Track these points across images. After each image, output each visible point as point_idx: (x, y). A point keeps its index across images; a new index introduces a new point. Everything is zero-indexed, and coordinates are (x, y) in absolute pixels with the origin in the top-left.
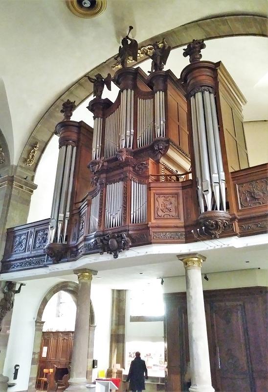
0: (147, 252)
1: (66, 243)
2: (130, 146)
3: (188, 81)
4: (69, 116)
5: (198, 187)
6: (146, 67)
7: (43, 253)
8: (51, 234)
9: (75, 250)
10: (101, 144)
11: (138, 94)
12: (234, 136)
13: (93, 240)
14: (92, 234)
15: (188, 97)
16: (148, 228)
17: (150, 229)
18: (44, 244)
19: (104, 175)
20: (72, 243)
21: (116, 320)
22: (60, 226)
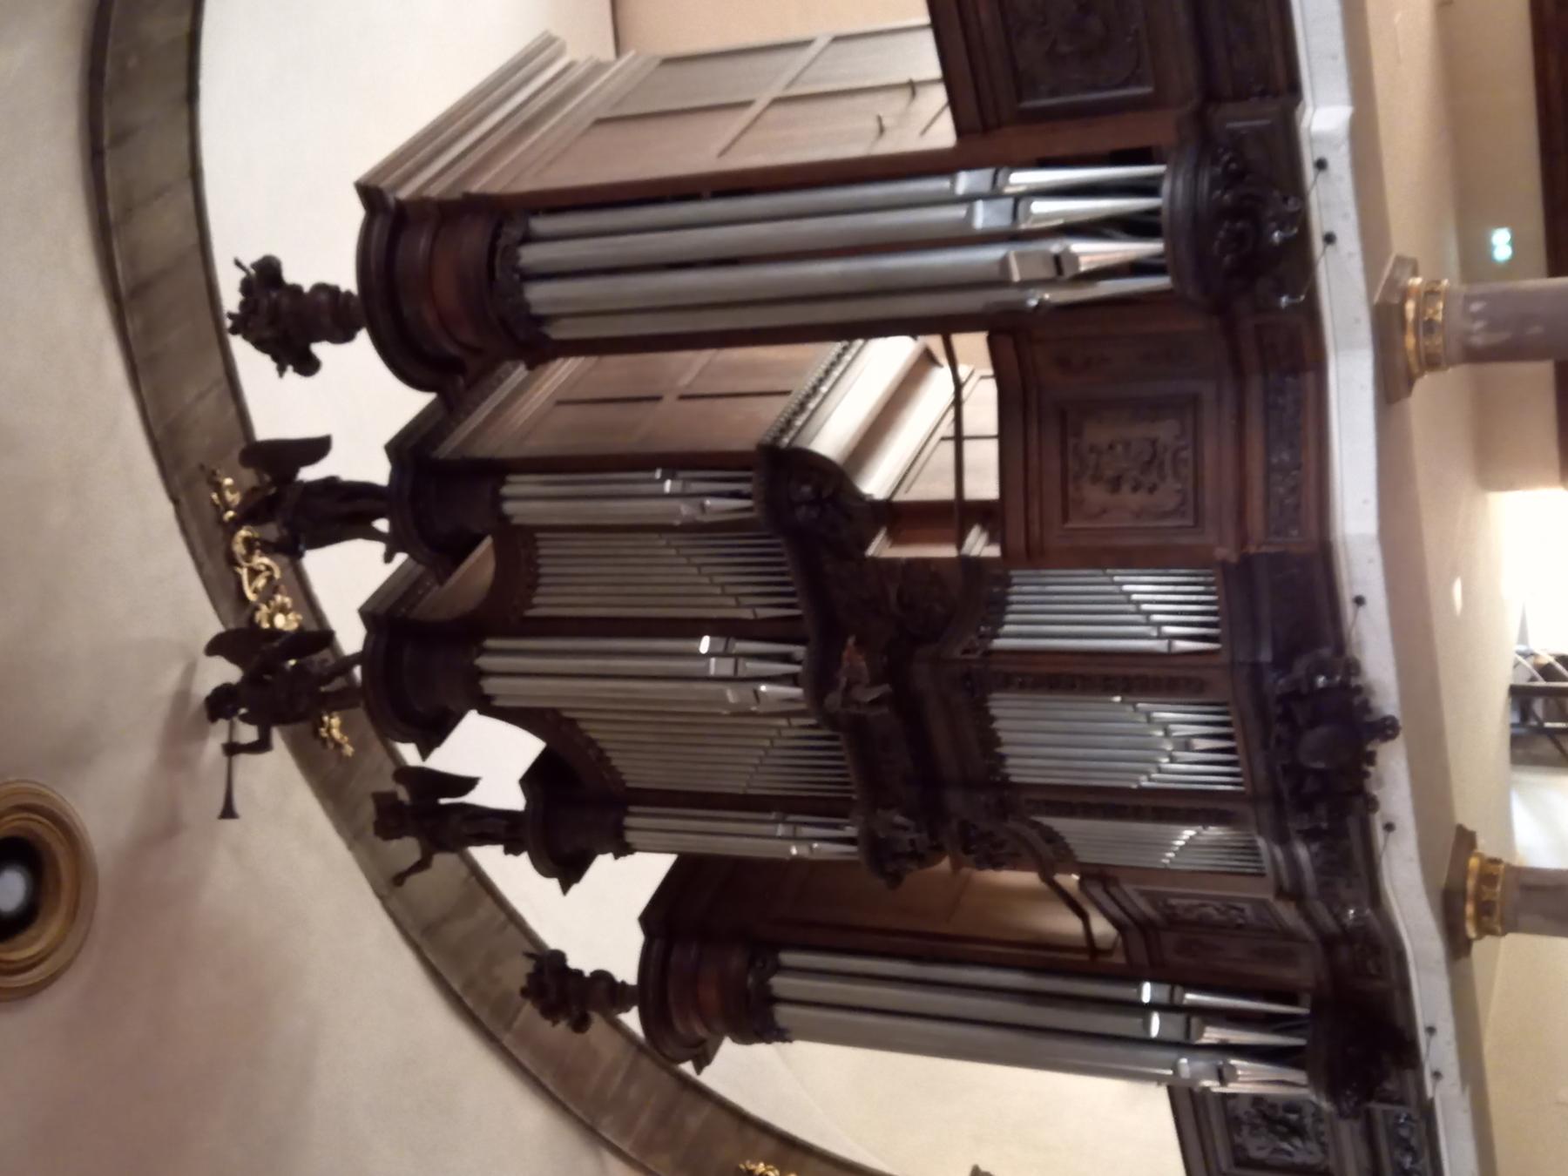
0: (1371, 561)
1: (1307, 998)
2: (786, 658)
3: (452, 350)
4: (601, 991)
5: (1033, 303)
6: (348, 578)
7: (1357, 1125)
8: (1249, 1079)
9: (1344, 954)
10: (773, 816)
11: (508, 614)
12: (748, 115)
13: (1302, 852)
14: (1265, 856)
15: (538, 347)
16: (1246, 562)
17: (1252, 549)
18: (1309, 1110)
19: (955, 800)
20: (1304, 971)
21: (1229, 905)
22: (1212, 1035)
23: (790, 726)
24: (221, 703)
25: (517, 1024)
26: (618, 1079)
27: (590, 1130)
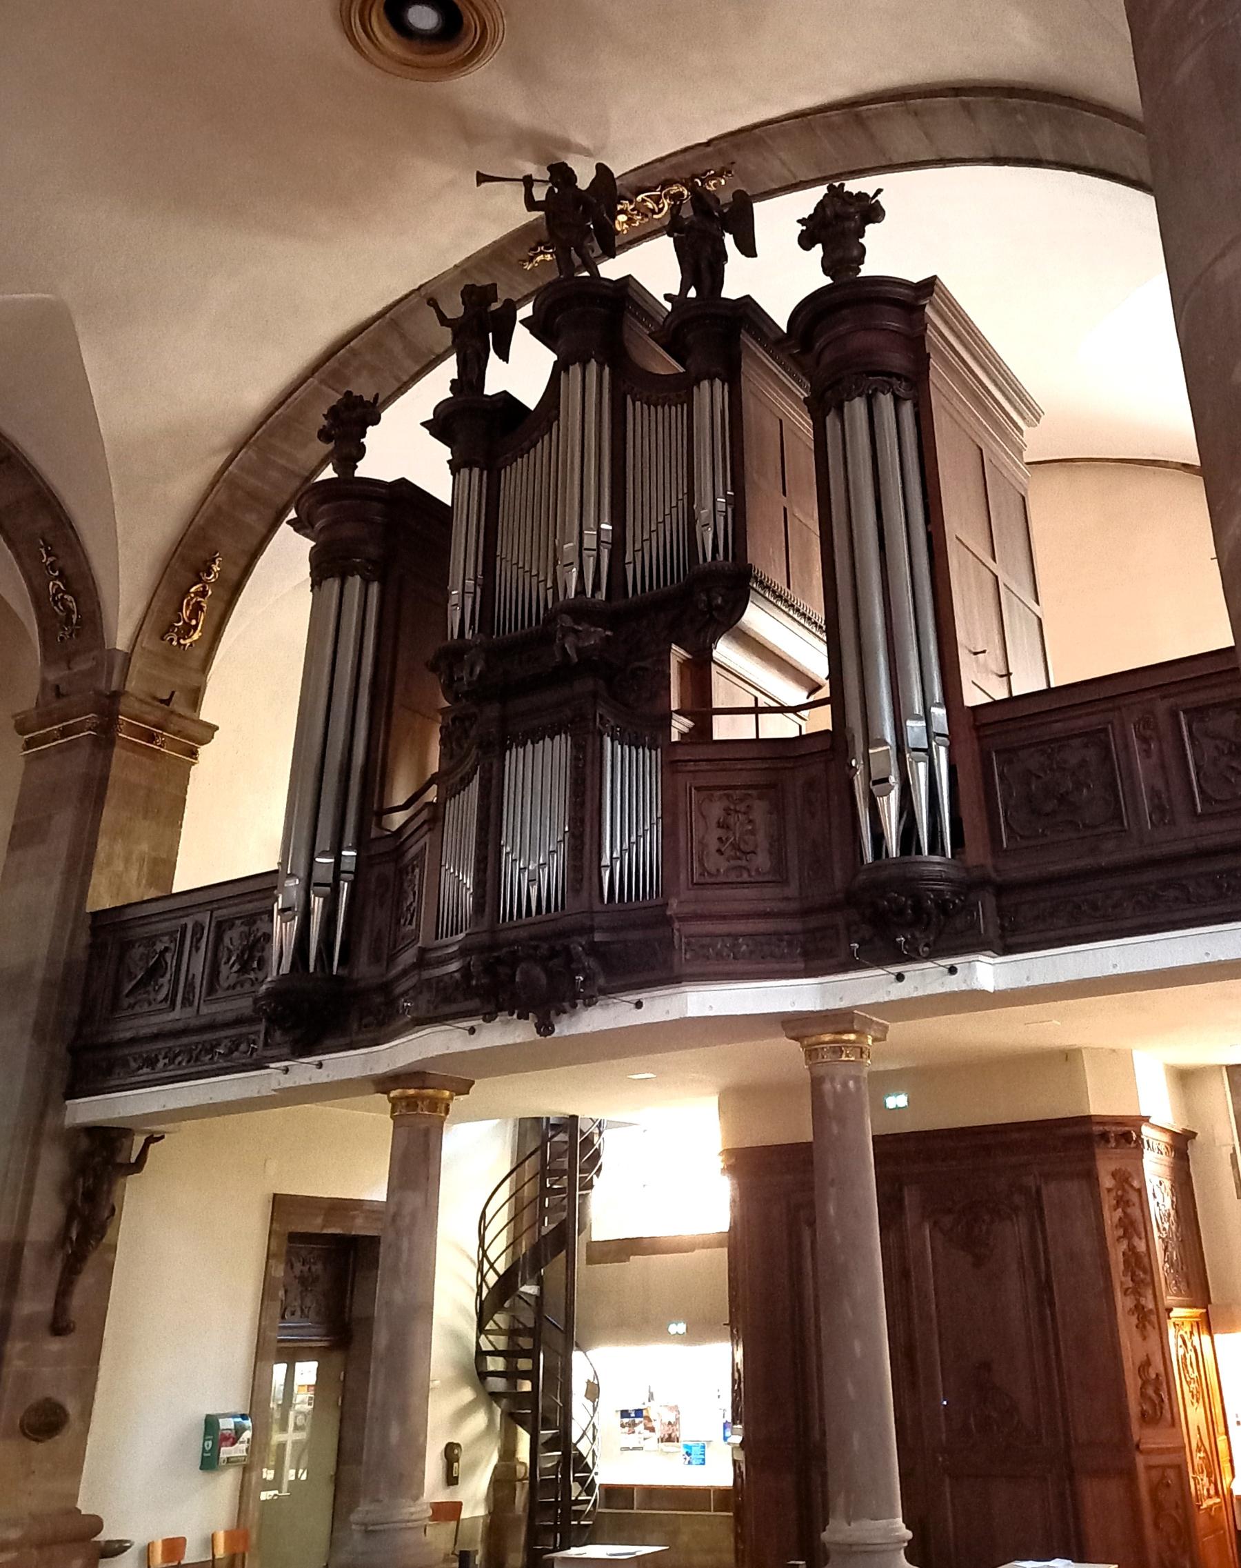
23: (547, 589)
24: (561, 174)
25: (324, 388)
26: (282, 462)
27: (245, 442)
